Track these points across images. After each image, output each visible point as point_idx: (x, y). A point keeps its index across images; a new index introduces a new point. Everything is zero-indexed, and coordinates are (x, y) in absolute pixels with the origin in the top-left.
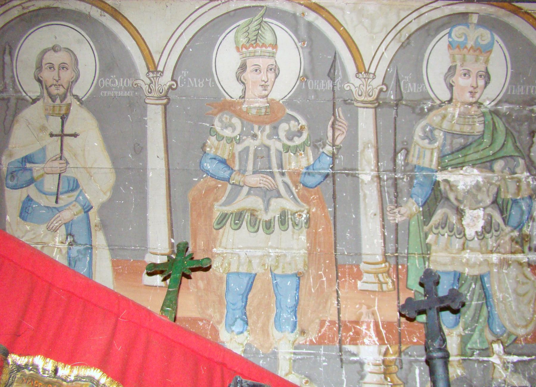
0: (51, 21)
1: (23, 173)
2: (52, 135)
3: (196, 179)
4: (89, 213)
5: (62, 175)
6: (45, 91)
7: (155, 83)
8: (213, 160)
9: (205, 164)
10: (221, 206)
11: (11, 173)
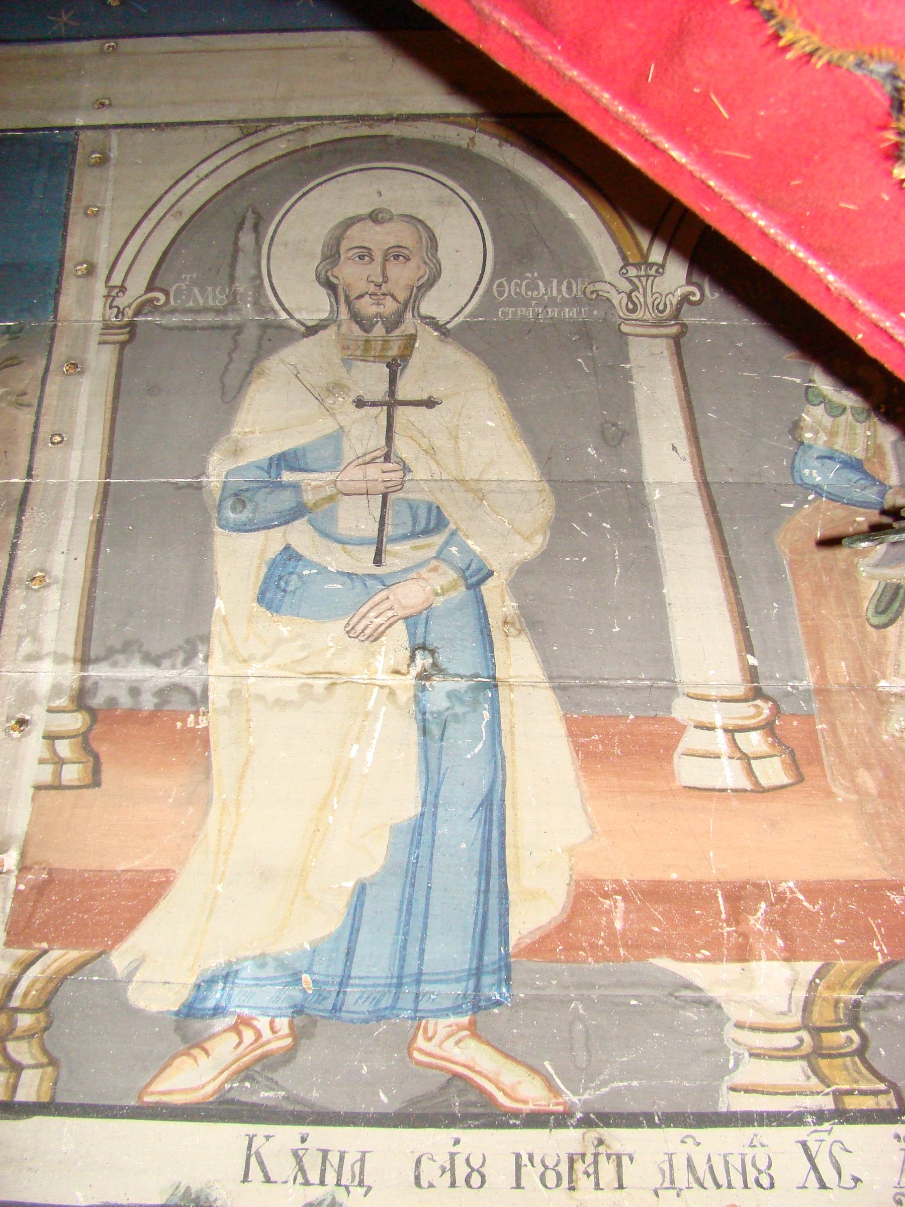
0: (368, 161)
1: (270, 493)
2: (360, 403)
3: (791, 505)
4: (483, 588)
5: (391, 497)
6: (343, 309)
7: (645, 289)
8: (827, 461)
9: (807, 471)
10: (876, 566)
11: (236, 495)
